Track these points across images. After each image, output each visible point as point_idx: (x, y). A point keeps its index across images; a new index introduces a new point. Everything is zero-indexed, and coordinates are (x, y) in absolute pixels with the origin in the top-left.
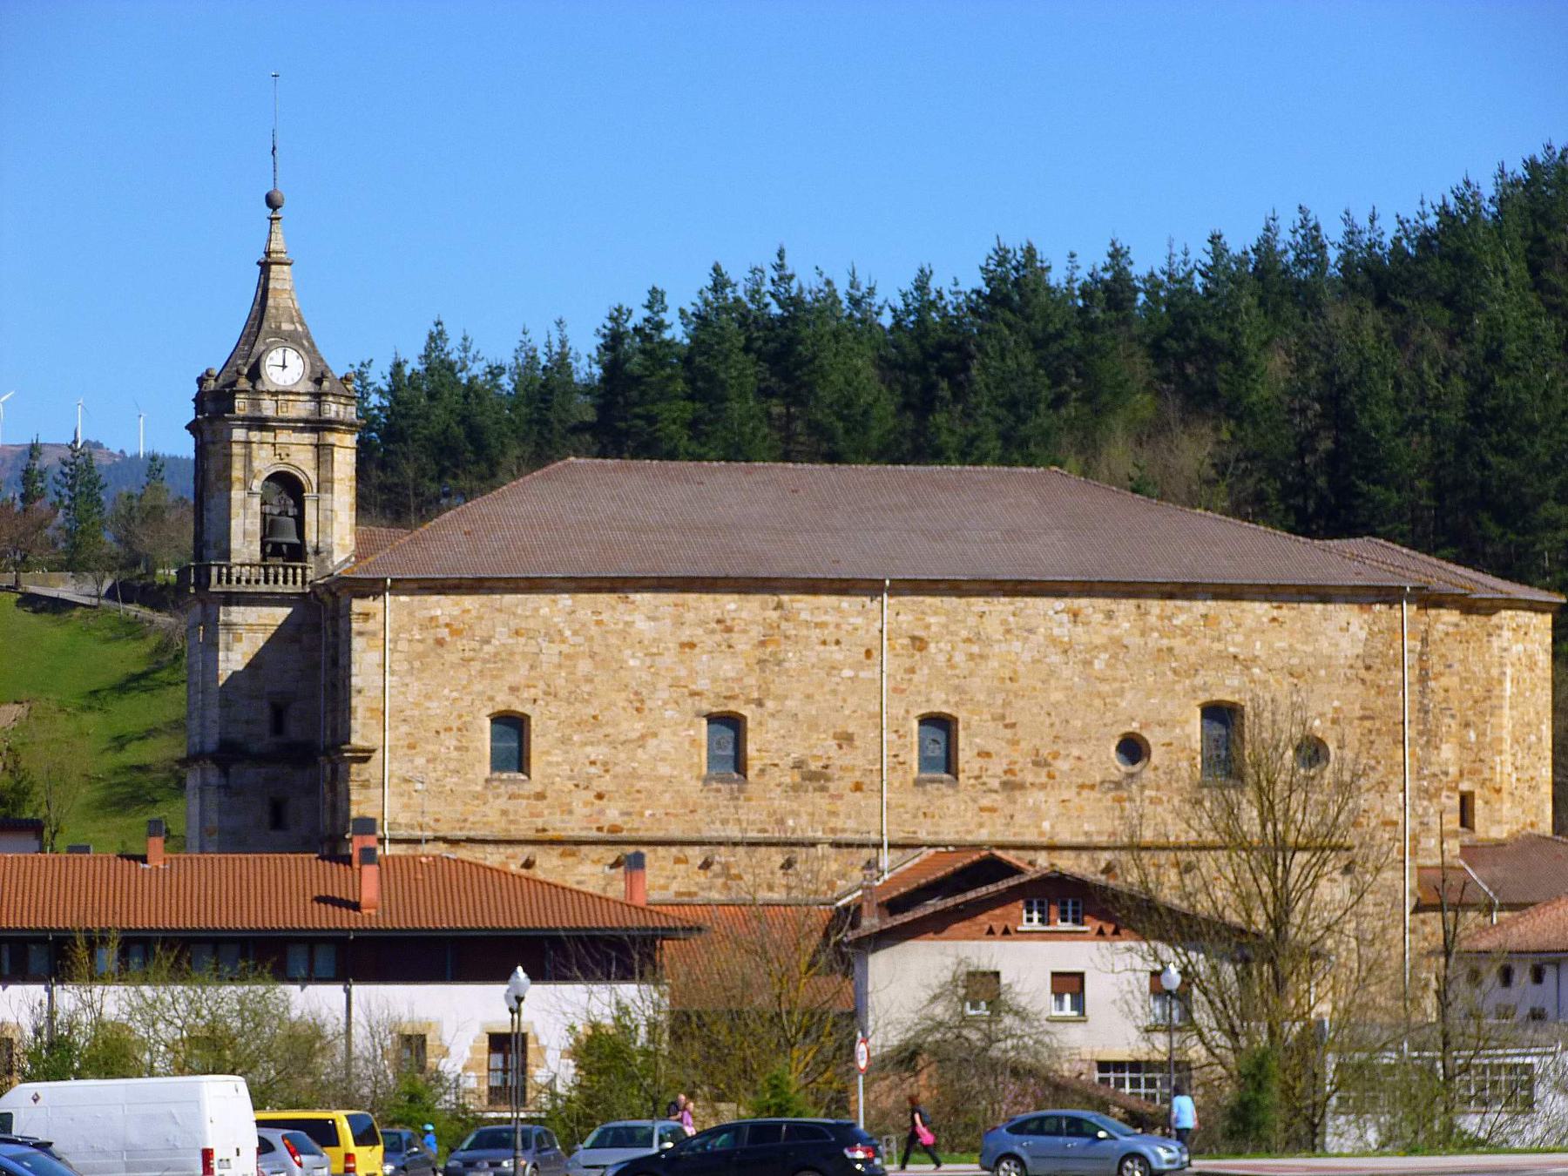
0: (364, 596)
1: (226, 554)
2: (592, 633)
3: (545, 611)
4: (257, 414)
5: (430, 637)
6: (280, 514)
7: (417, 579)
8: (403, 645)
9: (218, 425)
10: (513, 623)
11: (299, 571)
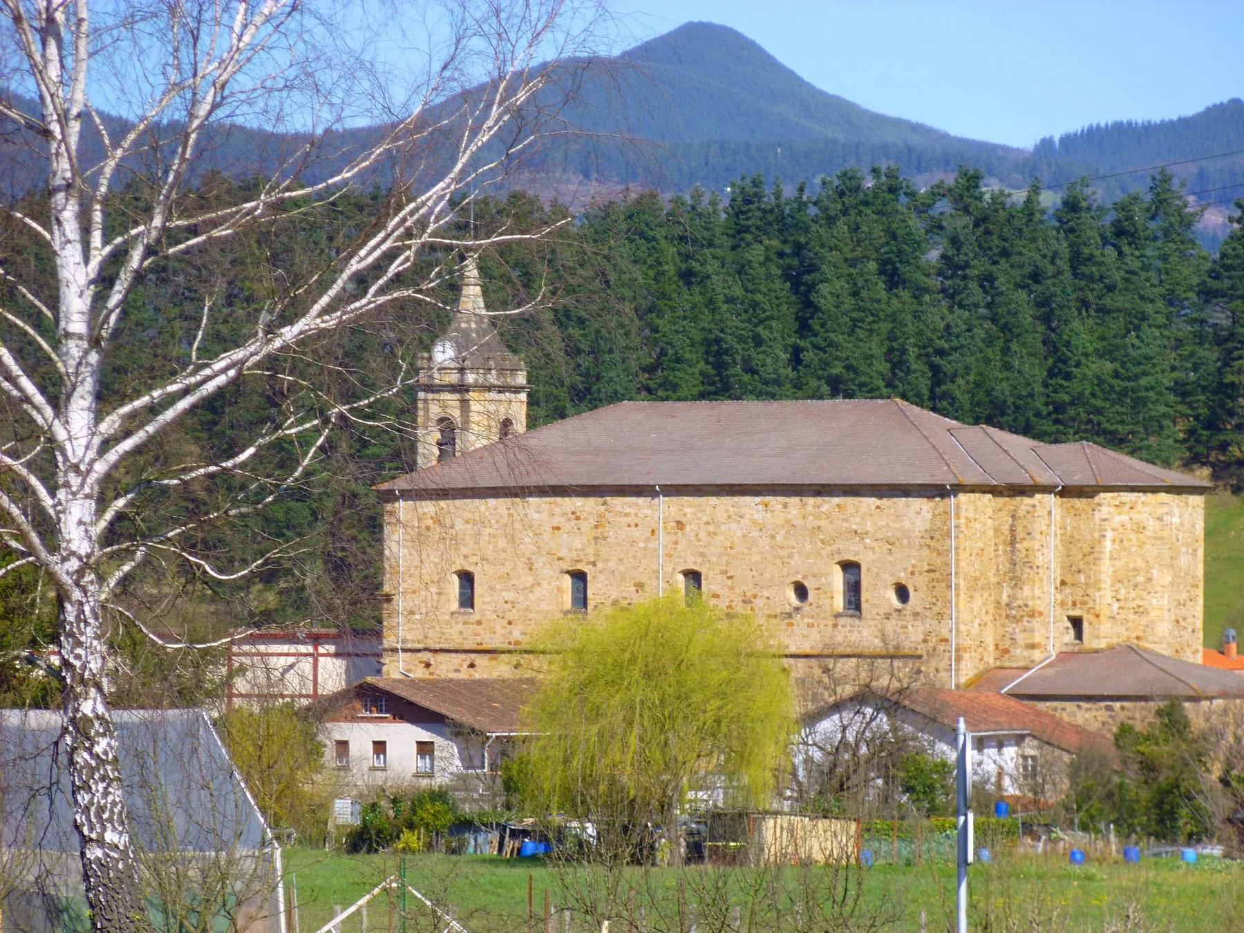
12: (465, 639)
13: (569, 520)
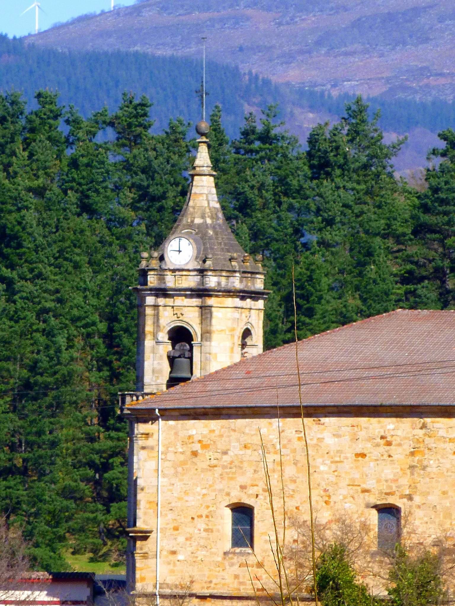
0: (145, 421)
4: (163, 286)
12: (241, 583)
13: (378, 445)
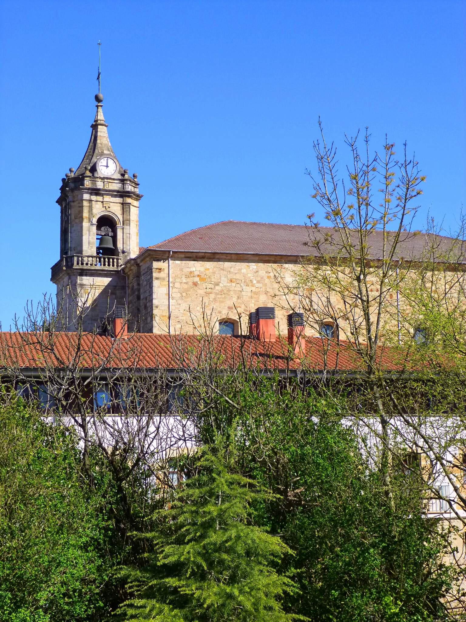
0: (158, 260)
1: (81, 252)
2: (266, 282)
3: (244, 271)
4: (95, 187)
5: (190, 280)
6: (105, 235)
7: (184, 252)
8: (177, 285)
9: (76, 192)
10: (230, 276)
11: (115, 260)
